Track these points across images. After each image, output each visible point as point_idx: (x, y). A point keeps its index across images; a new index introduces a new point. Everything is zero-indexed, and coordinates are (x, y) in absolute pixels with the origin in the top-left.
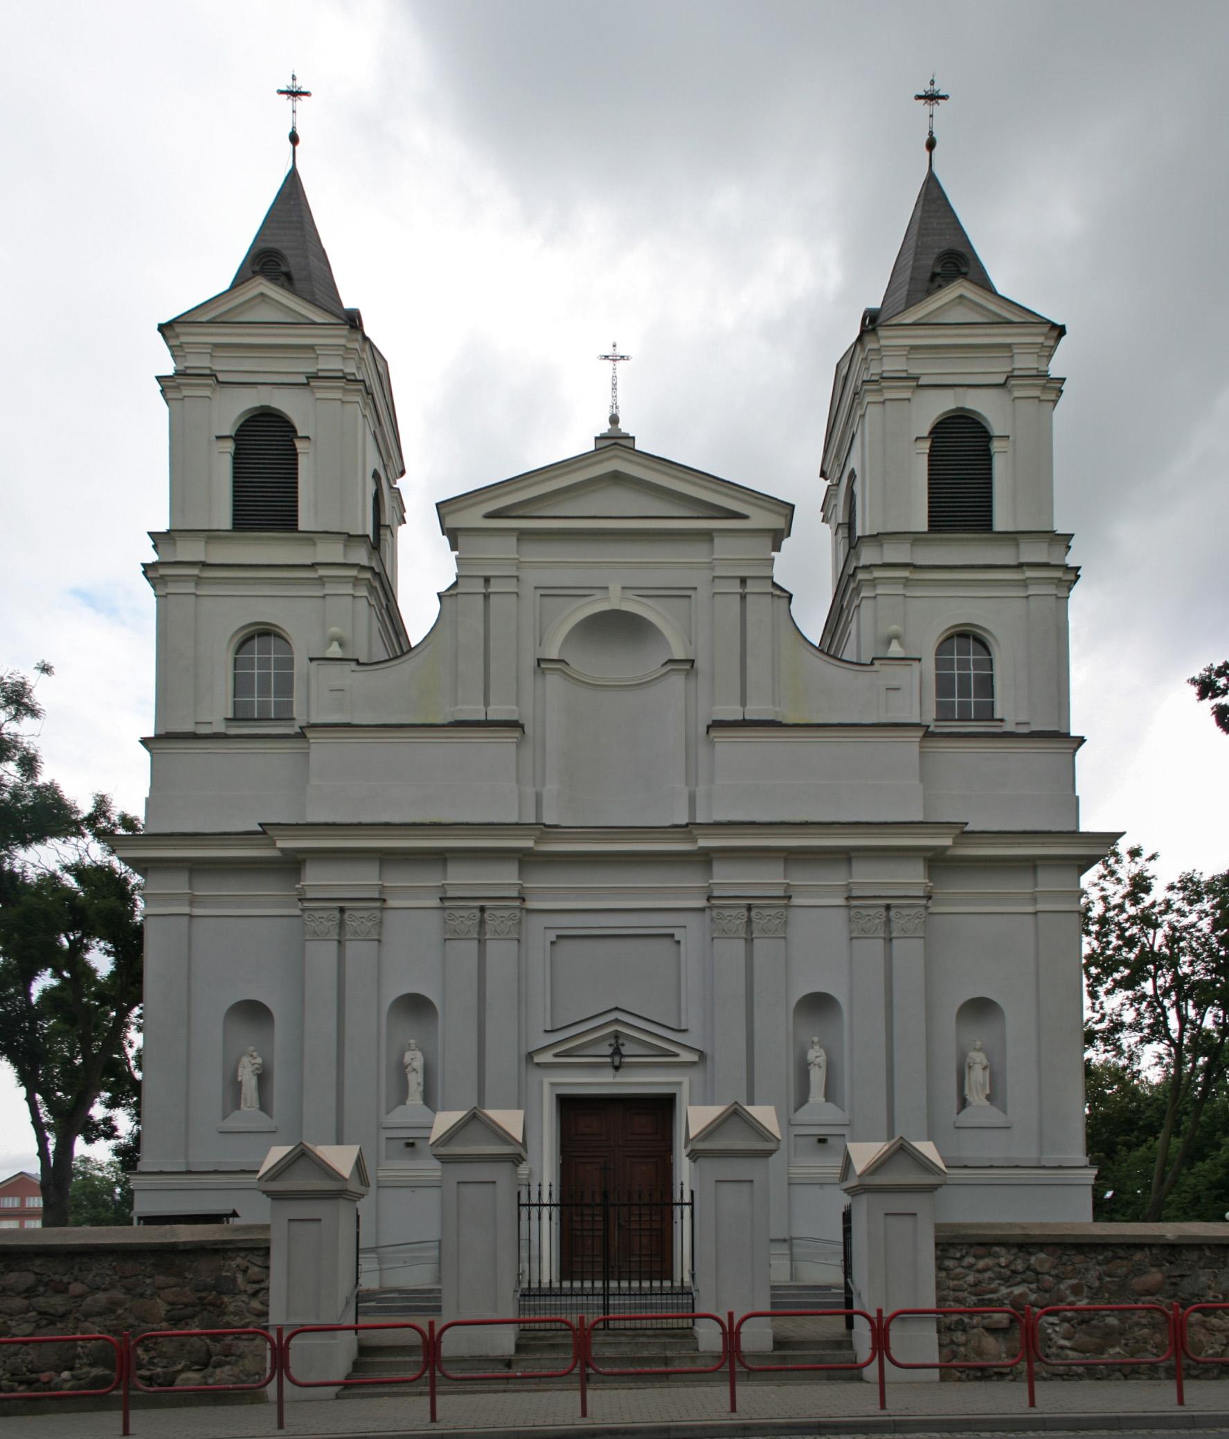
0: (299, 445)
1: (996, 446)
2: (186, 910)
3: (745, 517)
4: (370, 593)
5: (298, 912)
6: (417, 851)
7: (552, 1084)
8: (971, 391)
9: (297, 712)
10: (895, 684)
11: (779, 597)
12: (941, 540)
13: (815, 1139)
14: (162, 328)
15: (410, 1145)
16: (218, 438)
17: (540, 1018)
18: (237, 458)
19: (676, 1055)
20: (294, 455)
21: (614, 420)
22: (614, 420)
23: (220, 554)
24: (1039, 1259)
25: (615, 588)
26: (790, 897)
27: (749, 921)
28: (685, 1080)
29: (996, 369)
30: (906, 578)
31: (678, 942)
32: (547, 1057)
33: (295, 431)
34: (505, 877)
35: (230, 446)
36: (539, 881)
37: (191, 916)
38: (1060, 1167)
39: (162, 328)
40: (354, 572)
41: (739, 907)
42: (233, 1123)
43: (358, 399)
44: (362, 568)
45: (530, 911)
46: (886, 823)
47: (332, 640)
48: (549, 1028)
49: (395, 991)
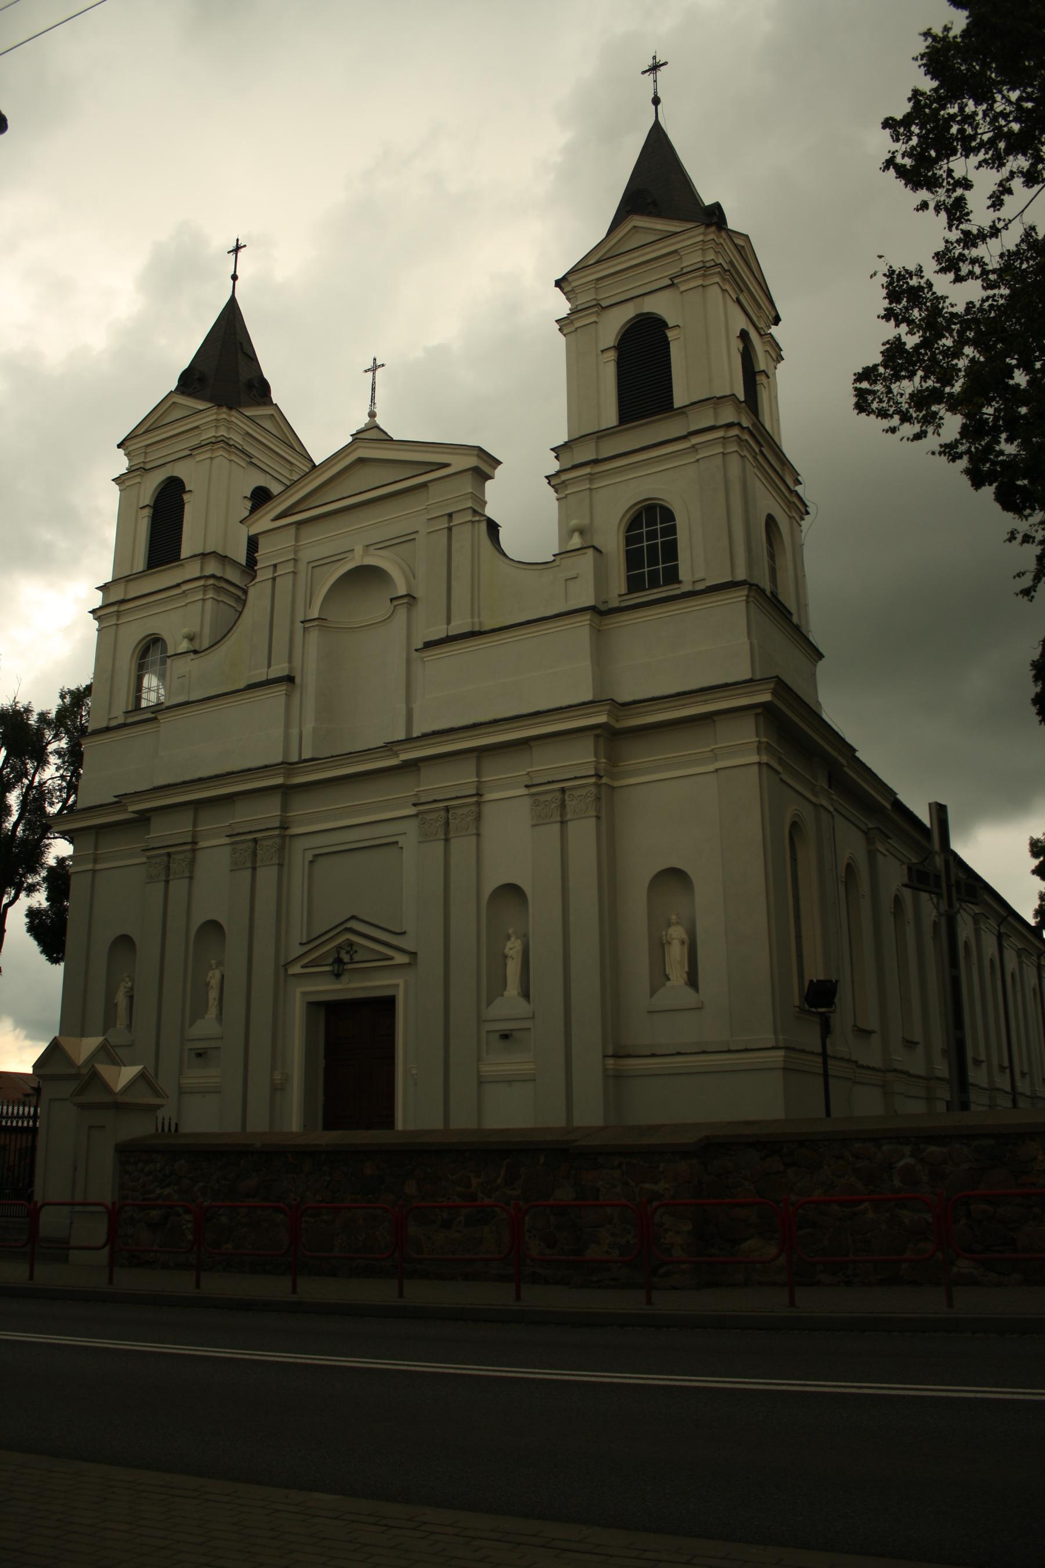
1: (671, 334)
2: (90, 867)
3: (447, 465)
4: (740, 446)
5: (144, 860)
7: (304, 994)
8: (647, 299)
9: (684, 573)
10: (572, 574)
11: (479, 521)
12: (174, 567)
13: (497, 1035)
14: (558, 283)
15: (199, 1055)
16: (602, 351)
17: (297, 934)
19: (392, 958)
20: (666, 344)
21: (372, 415)
22: (372, 415)
23: (609, 448)
26: (196, 843)
27: (563, 802)
29: (660, 276)
30: (724, 438)
31: (402, 848)
32: (296, 969)
33: (667, 325)
35: (612, 355)
38: (747, 1050)
39: (558, 283)
40: (720, 434)
41: (554, 791)
43: (717, 279)
44: (729, 426)
46: (561, 708)
47: (573, 531)
48: (305, 941)
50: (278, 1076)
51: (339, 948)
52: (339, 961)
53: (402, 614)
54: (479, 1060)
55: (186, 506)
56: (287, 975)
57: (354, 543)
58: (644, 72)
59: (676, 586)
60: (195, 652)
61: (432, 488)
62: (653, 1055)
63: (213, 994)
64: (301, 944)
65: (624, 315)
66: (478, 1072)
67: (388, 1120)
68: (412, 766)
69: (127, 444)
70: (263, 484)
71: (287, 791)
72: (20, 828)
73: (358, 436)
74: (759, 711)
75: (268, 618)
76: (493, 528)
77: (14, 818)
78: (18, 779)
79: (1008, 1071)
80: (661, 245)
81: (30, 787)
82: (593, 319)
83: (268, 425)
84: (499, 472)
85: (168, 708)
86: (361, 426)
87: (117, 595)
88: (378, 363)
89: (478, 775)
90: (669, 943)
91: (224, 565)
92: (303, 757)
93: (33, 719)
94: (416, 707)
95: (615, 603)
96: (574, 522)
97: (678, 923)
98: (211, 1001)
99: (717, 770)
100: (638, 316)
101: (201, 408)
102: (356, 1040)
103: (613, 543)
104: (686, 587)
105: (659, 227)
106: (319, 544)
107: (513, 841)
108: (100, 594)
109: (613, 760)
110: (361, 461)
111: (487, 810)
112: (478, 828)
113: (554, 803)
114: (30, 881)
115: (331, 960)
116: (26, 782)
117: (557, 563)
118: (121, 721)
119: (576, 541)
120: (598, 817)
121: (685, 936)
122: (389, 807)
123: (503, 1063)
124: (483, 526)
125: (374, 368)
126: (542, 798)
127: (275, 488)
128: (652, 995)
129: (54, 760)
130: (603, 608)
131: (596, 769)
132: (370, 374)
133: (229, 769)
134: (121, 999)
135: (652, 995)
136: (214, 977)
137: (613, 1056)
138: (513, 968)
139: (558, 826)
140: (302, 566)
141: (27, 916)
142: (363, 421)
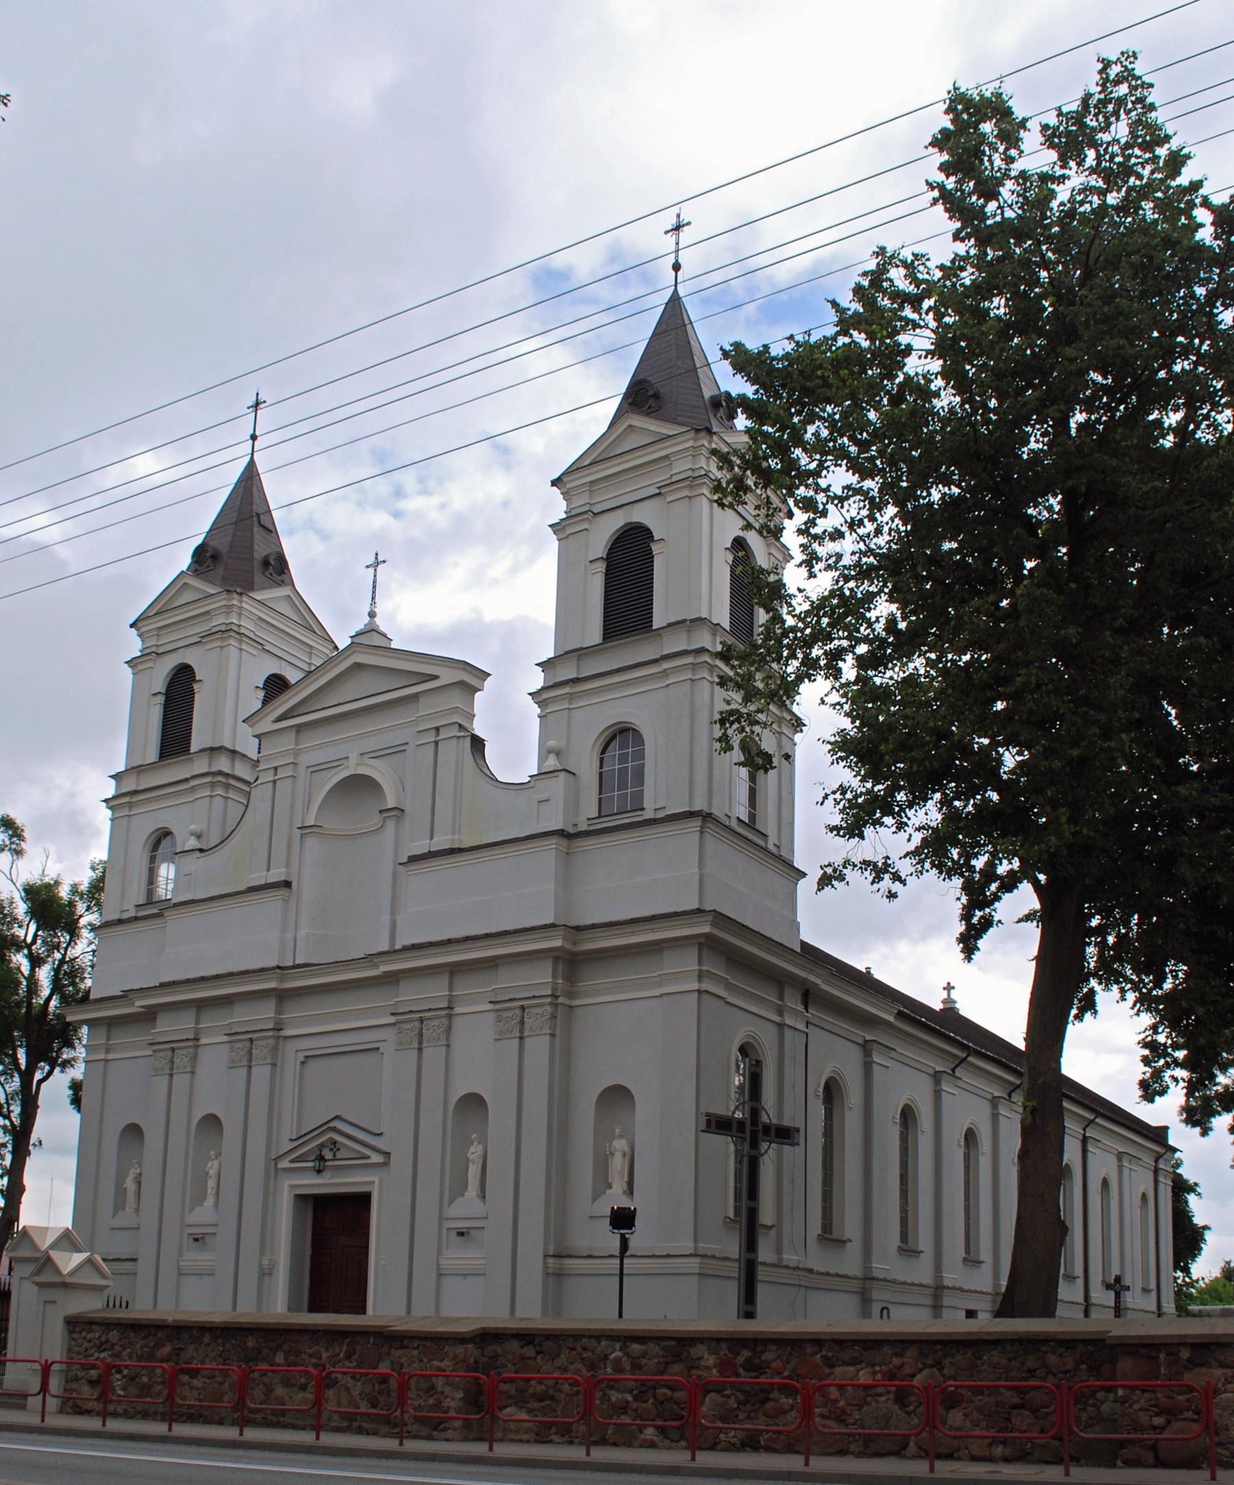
0: (655, 548)
2: (102, 1056)
3: (436, 677)
5: (149, 1052)
6: (209, 997)
7: (292, 1187)
8: (637, 506)
9: (648, 803)
10: (544, 796)
17: (288, 1131)
18: (167, 706)
19: (369, 1157)
20: (650, 557)
21: (372, 615)
22: (372, 615)
24: (114, 1335)
25: (353, 757)
28: (376, 1179)
29: (647, 483)
32: (285, 1164)
34: (265, 1013)
35: (601, 567)
36: (293, 1012)
37: (107, 1061)
38: (669, 1256)
41: (412, 1020)
42: (119, 1221)
45: (285, 1038)
49: (198, 1114)
50: (265, 1262)
51: (322, 1145)
52: (321, 1158)
53: (391, 826)
54: (439, 1253)
55: (197, 696)
56: (277, 1170)
57: (351, 750)
58: (667, 232)
59: (640, 813)
60: (201, 850)
61: (423, 701)
62: (590, 1257)
63: (211, 1184)
64: (291, 1140)
65: (615, 522)
66: (438, 1265)
67: (360, 1307)
68: (392, 979)
69: (139, 625)
70: (277, 672)
71: (282, 997)
72: (53, 1003)
73: (356, 640)
74: (702, 940)
75: (269, 822)
76: (478, 744)
77: (46, 992)
78: (50, 951)
79: (1154, 1294)
80: (653, 449)
81: (62, 961)
82: (586, 526)
83: (284, 608)
84: (488, 683)
85: (175, 905)
86: (360, 626)
87: (130, 785)
88: (380, 559)
89: (451, 990)
90: (612, 1154)
91: (233, 760)
92: (297, 962)
93: (64, 893)
94: (399, 918)
95: (583, 827)
96: (551, 743)
97: (621, 1137)
98: (209, 1190)
99: (662, 995)
100: (626, 524)
101: (213, 592)
102: (336, 1232)
103: (587, 767)
104: (649, 814)
105: (653, 428)
106: (318, 748)
107: (479, 1054)
108: (113, 782)
109: (571, 979)
110: (358, 666)
111: (458, 1023)
112: (448, 1039)
113: (515, 1017)
114: (65, 1056)
115: (313, 1158)
116: (58, 956)
117: (531, 785)
118: (132, 913)
119: (552, 763)
120: (553, 1035)
121: (627, 1149)
122: (368, 1014)
123: (458, 1256)
124: (468, 741)
125: (377, 563)
126: (505, 1014)
127: (293, 676)
128: (594, 1201)
129: (85, 933)
130: (572, 831)
131: (554, 989)
132: (372, 570)
133: (230, 970)
134: (130, 1184)
135: (594, 1201)
136: (212, 1167)
137: (553, 1256)
138: (473, 1172)
139: (517, 1041)
140: (302, 773)
141: (70, 1088)
142: (361, 623)
